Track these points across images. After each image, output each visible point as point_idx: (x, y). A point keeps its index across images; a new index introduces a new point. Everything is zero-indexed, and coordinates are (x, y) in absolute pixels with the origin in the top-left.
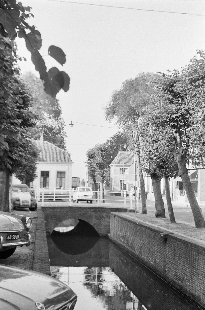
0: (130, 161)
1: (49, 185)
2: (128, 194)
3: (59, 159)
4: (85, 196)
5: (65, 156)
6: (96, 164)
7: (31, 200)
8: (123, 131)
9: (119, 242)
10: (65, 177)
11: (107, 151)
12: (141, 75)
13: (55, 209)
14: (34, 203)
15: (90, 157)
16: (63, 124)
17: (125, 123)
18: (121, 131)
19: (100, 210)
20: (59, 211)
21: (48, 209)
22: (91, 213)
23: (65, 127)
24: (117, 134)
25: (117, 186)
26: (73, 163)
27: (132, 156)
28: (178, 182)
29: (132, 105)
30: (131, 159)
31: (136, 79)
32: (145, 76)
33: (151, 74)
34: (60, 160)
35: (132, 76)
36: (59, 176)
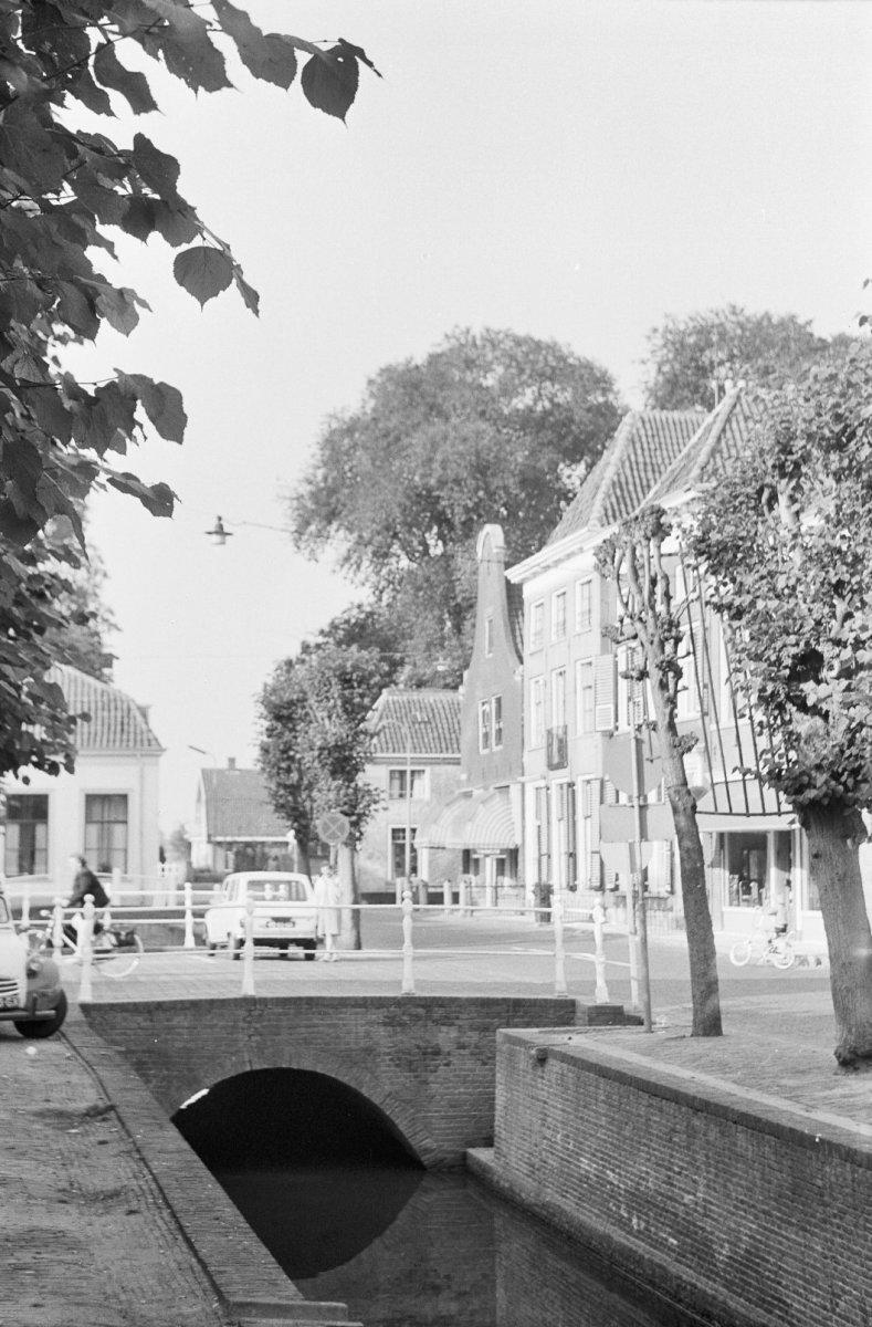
0: (436, 734)
1: (46, 863)
2: (441, 902)
3: (96, 734)
4: (277, 920)
5: (123, 717)
6: (316, 753)
7: (31, 974)
8: (373, 599)
9: (601, 1226)
10: (125, 822)
11: (372, 682)
12: (458, 340)
13: (161, 1015)
14: (49, 991)
15: (278, 718)
16: (96, 572)
17: (382, 555)
18: (365, 602)
19: (421, 1011)
20: (186, 1024)
21: (119, 1016)
22: (368, 1035)
23: (106, 583)
24: (346, 616)
25: (379, 858)
26: (165, 750)
27: (442, 711)
28: (721, 835)
29: (423, 476)
30: (440, 725)
31: (434, 359)
32: (475, 345)
33: (501, 336)
34: (98, 739)
35: (416, 347)
36: (96, 816)
